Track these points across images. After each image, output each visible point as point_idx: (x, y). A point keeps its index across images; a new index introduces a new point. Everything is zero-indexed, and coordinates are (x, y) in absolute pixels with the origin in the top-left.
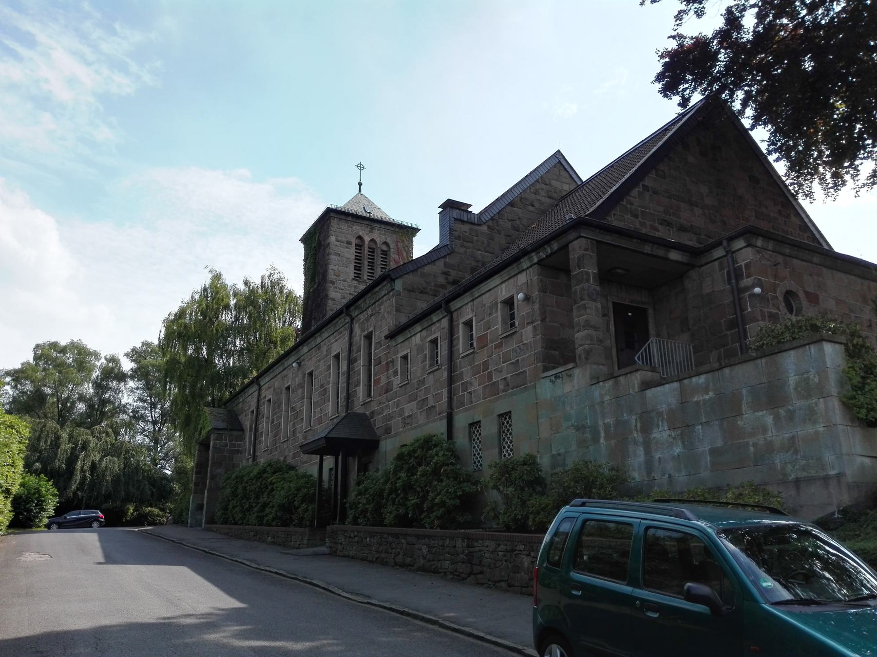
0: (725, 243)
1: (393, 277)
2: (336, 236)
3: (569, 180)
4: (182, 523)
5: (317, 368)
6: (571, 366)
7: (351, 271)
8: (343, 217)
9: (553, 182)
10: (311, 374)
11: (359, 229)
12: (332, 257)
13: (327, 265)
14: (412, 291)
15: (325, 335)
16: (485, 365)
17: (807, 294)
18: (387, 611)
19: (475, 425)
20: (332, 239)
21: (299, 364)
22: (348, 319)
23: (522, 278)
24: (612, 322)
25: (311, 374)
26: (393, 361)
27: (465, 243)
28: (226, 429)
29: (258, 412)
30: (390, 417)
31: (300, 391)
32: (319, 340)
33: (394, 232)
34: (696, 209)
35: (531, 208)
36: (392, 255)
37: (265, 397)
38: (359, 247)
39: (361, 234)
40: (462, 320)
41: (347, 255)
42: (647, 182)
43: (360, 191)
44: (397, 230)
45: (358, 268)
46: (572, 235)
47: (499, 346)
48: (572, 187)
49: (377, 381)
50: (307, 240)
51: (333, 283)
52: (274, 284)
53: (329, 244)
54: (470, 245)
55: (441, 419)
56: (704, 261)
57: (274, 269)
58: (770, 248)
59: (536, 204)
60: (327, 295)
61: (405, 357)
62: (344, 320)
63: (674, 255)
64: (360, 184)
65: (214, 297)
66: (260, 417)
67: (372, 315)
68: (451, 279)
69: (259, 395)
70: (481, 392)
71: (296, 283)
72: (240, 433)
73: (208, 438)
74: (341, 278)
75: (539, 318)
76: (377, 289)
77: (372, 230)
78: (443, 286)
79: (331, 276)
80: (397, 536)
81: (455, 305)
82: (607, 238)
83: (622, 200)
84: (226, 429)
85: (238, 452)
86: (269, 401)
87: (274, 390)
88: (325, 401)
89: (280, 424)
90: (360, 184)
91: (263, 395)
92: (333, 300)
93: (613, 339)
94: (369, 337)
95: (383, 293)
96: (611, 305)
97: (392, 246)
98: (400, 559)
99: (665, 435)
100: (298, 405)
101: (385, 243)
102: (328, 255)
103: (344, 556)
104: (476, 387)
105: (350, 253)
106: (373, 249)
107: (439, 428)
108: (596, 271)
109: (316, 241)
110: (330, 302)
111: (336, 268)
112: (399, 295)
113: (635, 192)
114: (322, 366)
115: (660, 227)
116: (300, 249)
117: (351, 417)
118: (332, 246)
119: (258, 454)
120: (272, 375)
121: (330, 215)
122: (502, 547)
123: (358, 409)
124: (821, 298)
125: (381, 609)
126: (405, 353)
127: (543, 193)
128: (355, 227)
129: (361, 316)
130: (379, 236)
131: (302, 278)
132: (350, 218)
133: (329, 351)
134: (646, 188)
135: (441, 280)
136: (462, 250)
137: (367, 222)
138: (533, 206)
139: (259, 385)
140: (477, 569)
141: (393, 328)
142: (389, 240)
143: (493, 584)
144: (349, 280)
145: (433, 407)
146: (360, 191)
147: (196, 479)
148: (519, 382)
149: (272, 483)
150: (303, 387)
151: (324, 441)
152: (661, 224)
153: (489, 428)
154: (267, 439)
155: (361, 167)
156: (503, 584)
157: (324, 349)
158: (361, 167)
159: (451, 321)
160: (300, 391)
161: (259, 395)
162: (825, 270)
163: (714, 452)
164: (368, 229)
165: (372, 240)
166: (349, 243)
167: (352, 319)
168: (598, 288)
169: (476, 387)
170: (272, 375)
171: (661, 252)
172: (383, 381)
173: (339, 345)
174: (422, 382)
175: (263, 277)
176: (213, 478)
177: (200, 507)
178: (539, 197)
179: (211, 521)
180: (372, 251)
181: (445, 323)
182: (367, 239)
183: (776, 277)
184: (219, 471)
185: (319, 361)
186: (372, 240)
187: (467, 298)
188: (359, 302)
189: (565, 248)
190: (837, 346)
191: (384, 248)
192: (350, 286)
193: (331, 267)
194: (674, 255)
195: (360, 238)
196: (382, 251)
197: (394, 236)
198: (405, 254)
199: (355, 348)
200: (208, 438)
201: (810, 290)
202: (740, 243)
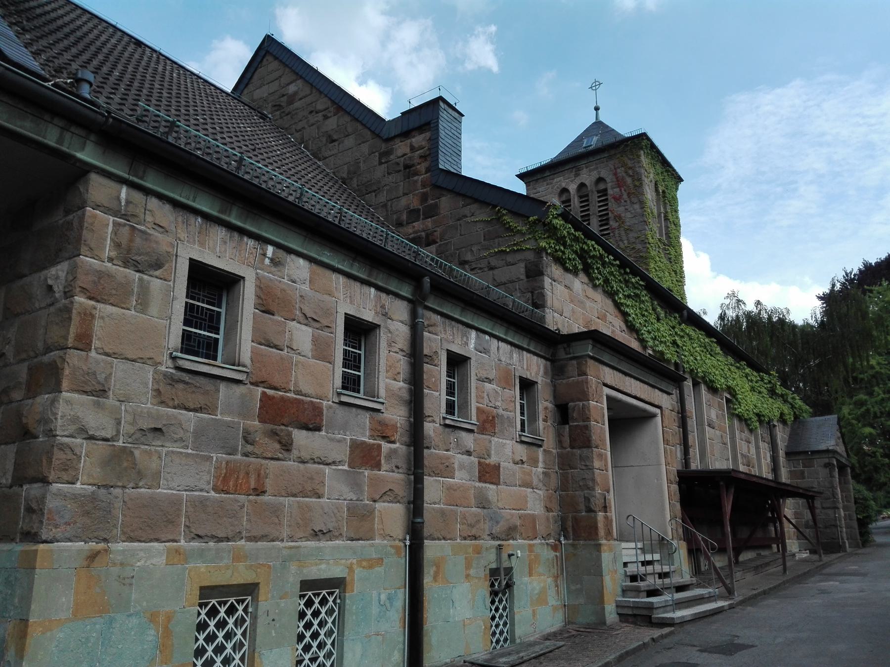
64: (597, 109)
90: (597, 109)
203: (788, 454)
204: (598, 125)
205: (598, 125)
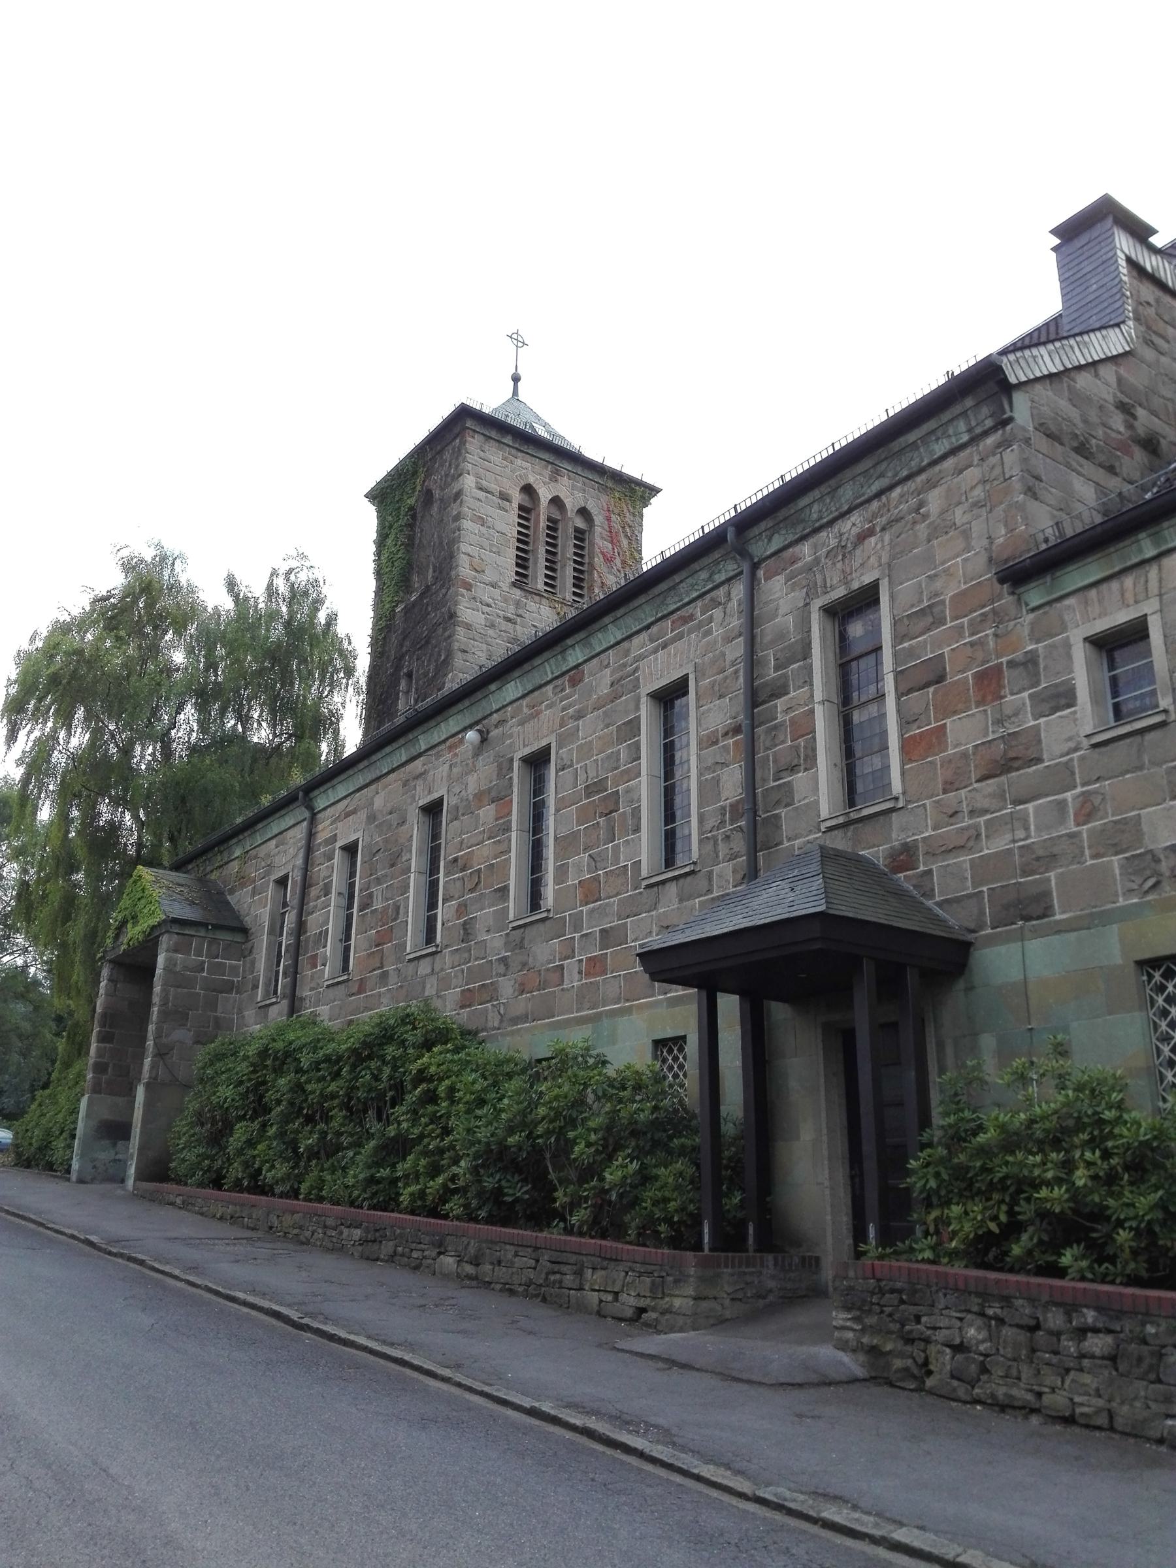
2: (478, 476)
4: (50, 1167)
8: (493, 434)
12: (466, 524)
13: (454, 541)
20: (469, 482)
25: (537, 762)
28: (204, 925)
31: (487, 813)
33: (604, 489)
36: (598, 540)
37: (334, 839)
38: (525, 512)
39: (531, 480)
43: (515, 392)
44: (610, 484)
45: (522, 562)
50: (381, 495)
51: (468, 587)
52: (297, 595)
53: (458, 495)
57: (303, 556)
60: (452, 615)
64: (516, 379)
66: (314, 892)
67: (862, 537)
69: (311, 835)
72: (239, 938)
73: (150, 944)
74: (487, 579)
77: (555, 475)
79: (464, 570)
84: (204, 925)
85: (229, 987)
87: (372, 818)
90: (516, 379)
92: (468, 627)
95: (940, 448)
97: (598, 519)
101: (583, 512)
102: (458, 518)
105: (507, 523)
109: (413, 502)
110: (460, 631)
111: (469, 549)
116: (368, 518)
118: (468, 500)
119: (305, 992)
120: (360, 780)
121: (464, 419)
125: (208, 1295)
128: (519, 462)
130: (572, 492)
131: (371, 584)
132: (508, 440)
133: (624, 684)
137: (546, 456)
139: (310, 808)
142: (591, 506)
144: (505, 586)
146: (515, 392)
147: (100, 1053)
149: (421, 1077)
155: (517, 340)
158: (517, 340)
160: (487, 813)
161: (311, 835)
164: (547, 473)
165: (556, 501)
166: (505, 497)
170: (360, 780)
175: (274, 573)
176: (161, 1054)
177: (115, 1131)
179: (158, 1171)
180: (553, 525)
182: (545, 495)
185: (579, 716)
186: (556, 501)
188: (803, 502)
191: (580, 523)
192: (506, 601)
193: (464, 547)
195: (528, 490)
196: (577, 530)
197: (604, 498)
198: (625, 542)
200: (150, 944)
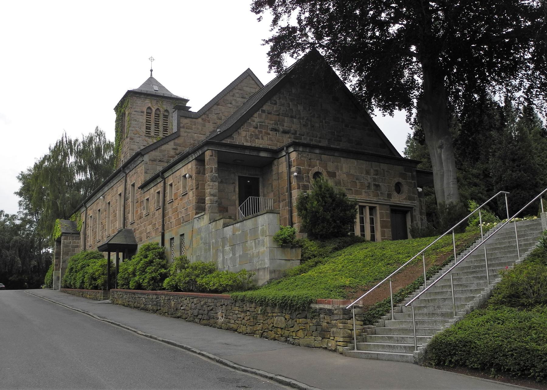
0: (285, 148)
1: (143, 153)
3: (255, 86)
5: (112, 200)
6: (203, 213)
7: (144, 129)
9: (244, 88)
10: (109, 203)
11: (148, 103)
14: (155, 160)
15: (115, 182)
16: (177, 208)
17: (328, 173)
18: (165, 344)
19: (172, 239)
21: (104, 197)
22: (124, 175)
23: (189, 166)
24: (237, 187)
25: (109, 203)
26: (143, 201)
27: (187, 130)
29: (85, 223)
30: (141, 233)
32: (112, 184)
34: (295, 120)
35: (229, 105)
38: (149, 114)
40: (169, 184)
41: (141, 120)
42: (264, 108)
45: (148, 128)
46: (206, 148)
47: (181, 200)
48: (257, 90)
49: (137, 211)
50: (116, 109)
54: (190, 131)
55: (158, 236)
56: (280, 156)
58: (308, 151)
59: (233, 102)
61: (148, 200)
62: (122, 175)
63: (263, 154)
64: (151, 71)
65: (61, 150)
68: (178, 152)
70: (174, 222)
71: (111, 136)
75: (195, 188)
76: (136, 159)
78: (173, 157)
80: (134, 293)
81: (166, 175)
82: (224, 150)
83: (248, 120)
85: (77, 247)
86: (91, 217)
88: (116, 221)
89: (96, 231)
90: (151, 71)
91: (88, 214)
93: (237, 196)
94: (133, 185)
95: (139, 162)
96: (237, 178)
98: (135, 305)
99: (228, 248)
100: (104, 221)
103: (135, 307)
104: (173, 220)
106: (158, 115)
107: (159, 240)
108: (216, 166)
112: (147, 163)
113: (256, 115)
114: (114, 201)
115: (271, 132)
117: (125, 231)
120: (92, 202)
121: (130, 94)
122: (166, 298)
123: (129, 227)
124: (337, 174)
126: (158, 190)
127: (237, 95)
129: (130, 173)
134: (263, 111)
135: (172, 153)
136: (186, 134)
138: (231, 103)
139: (86, 207)
140: (159, 308)
141: (143, 183)
142: (169, 109)
143: (164, 314)
145: (158, 228)
148: (186, 221)
150: (106, 211)
151: (106, 246)
152: (271, 130)
153: (177, 242)
154: (90, 239)
155: (152, 59)
156: (166, 314)
157: (115, 189)
158: (152, 59)
159: (165, 183)
162: (342, 159)
163: (240, 256)
166: (143, 112)
167: (126, 175)
168: (217, 175)
169: (173, 220)
171: (255, 153)
172: (139, 212)
173: (121, 189)
174: (154, 214)
178: (235, 98)
181: (162, 184)
183: (309, 166)
184: (67, 257)
187: (170, 172)
189: (203, 154)
190: (275, 214)
194: (263, 154)
199: (127, 191)
201: (330, 170)
202: (291, 149)
203: (79, 234)
204: (151, 81)
205: (151, 81)
